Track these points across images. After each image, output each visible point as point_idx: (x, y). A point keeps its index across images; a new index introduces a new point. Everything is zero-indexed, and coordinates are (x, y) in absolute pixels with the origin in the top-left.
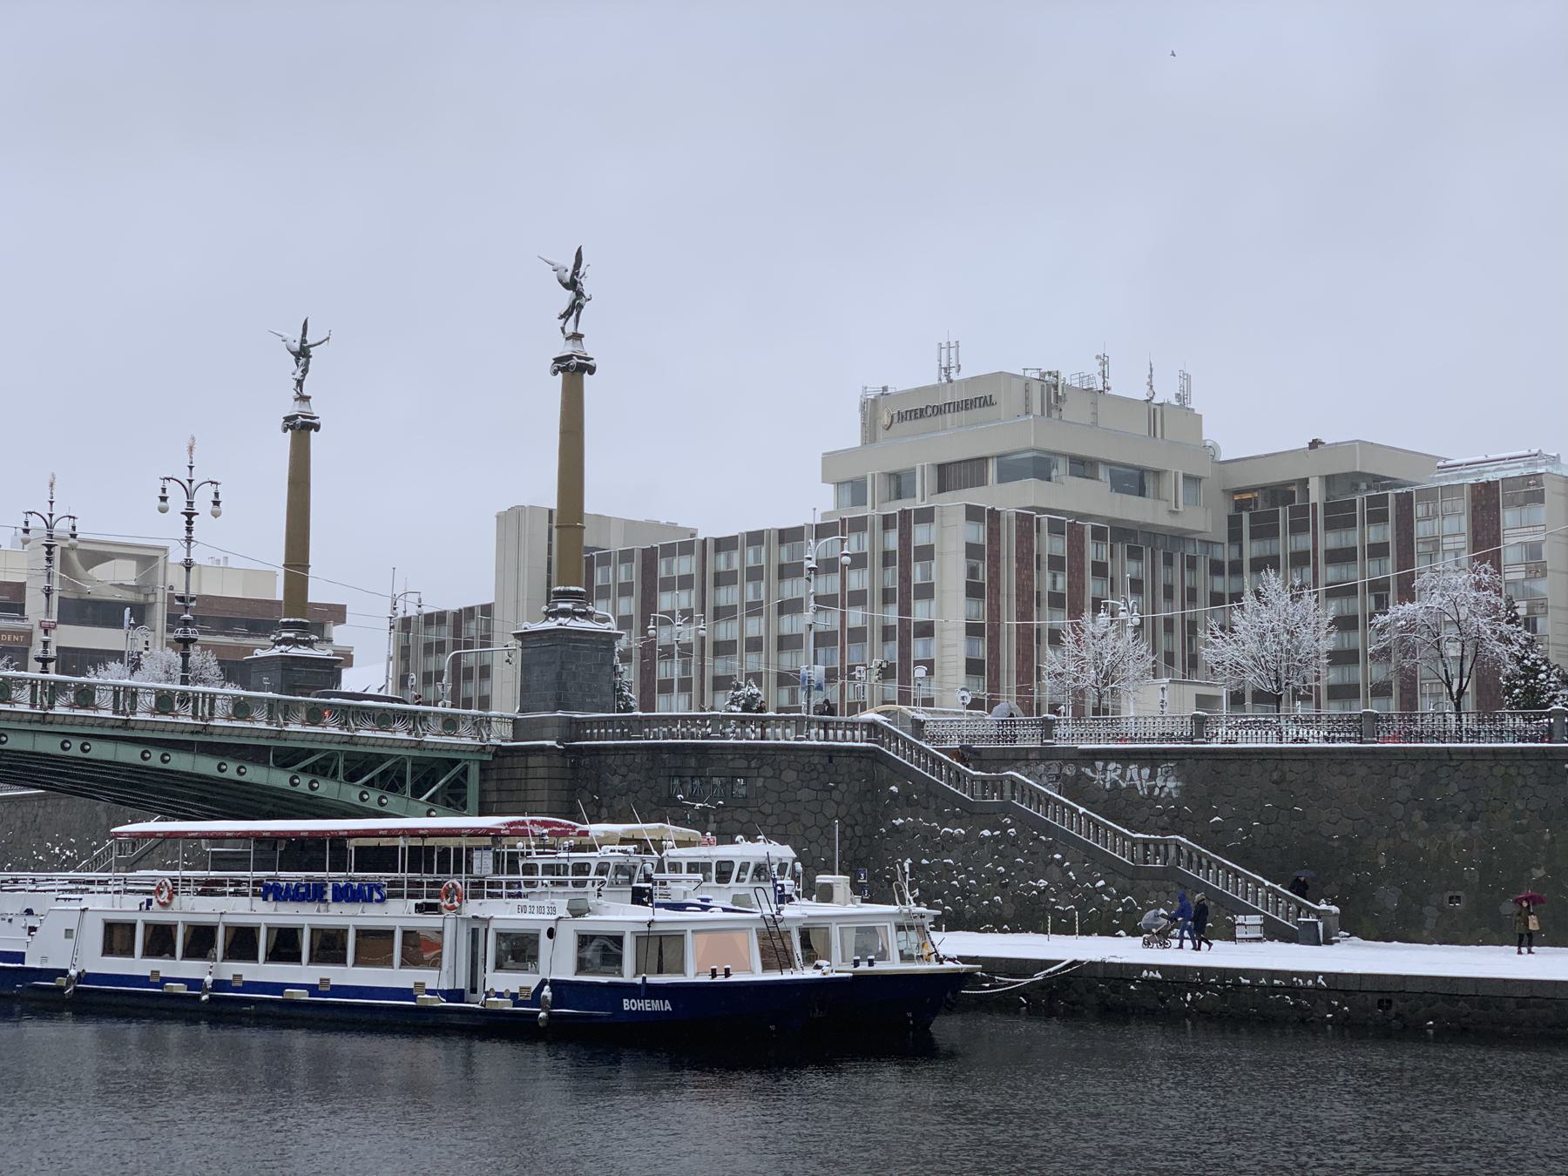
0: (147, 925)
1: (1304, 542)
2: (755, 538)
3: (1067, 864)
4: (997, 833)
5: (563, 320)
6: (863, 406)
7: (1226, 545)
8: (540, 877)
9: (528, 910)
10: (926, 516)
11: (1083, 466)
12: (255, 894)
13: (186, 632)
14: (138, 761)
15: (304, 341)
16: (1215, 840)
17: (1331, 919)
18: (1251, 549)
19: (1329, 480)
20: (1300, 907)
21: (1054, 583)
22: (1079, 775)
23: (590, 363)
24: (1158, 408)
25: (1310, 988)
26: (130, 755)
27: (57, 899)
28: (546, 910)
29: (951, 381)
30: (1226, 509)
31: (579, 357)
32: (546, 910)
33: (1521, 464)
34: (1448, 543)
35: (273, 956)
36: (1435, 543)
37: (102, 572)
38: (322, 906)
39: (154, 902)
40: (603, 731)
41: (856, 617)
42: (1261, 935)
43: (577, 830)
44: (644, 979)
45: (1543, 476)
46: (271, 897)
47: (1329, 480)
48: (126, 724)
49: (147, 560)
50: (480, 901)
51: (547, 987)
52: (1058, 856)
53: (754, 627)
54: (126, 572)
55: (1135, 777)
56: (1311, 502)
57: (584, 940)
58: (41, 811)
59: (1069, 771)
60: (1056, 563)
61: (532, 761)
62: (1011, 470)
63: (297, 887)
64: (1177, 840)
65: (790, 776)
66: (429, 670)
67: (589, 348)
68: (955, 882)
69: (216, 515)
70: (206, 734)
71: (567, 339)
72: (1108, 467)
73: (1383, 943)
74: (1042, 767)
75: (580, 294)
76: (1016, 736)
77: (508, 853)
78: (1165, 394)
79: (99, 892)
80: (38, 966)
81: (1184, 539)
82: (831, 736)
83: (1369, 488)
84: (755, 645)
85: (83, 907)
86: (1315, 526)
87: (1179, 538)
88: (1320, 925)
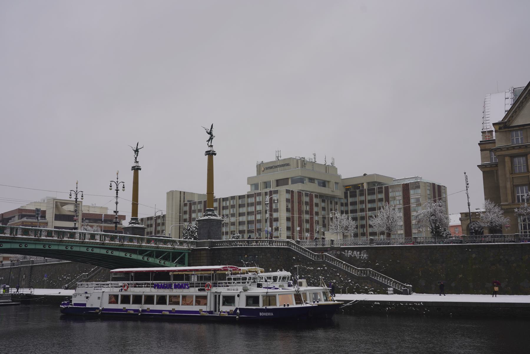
0: (122, 296)
1: (363, 198)
2: (233, 198)
3: (341, 276)
4: (322, 268)
5: (208, 142)
6: (257, 166)
7: (344, 199)
8: (232, 281)
9: (230, 290)
10: (276, 192)
11: (311, 180)
12: (152, 287)
13: (116, 220)
14: (106, 253)
15: (137, 148)
16: (377, 269)
17: (410, 288)
18: (350, 200)
19: (368, 183)
20: (402, 285)
21: (306, 208)
22: (341, 254)
23: (215, 152)
24: (327, 166)
25: (419, 305)
26: (104, 252)
27: (94, 289)
28: (235, 290)
29: (279, 160)
30: (344, 190)
31: (212, 151)
32: (235, 290)
33: (414, 179)
34: (397, 198)
35: (158, 303)
36: (394, 198)
38: (171, 290)
39: (123, 289)
40: (221, 244)
41: (258, 217)
42: (393, 293)
43: (238, 269)
44: (266, 307)
45: (420, 182)
46: (156, 288)
47: (368, 183)
48: (103, 244)
50: (216, 288)
51: (238, 310)
52: (338, 274)
53: (233, 219)
54: (71, 208)
55: (356, 254)
56: (364, 188)
57: (248, 298)
58: (60, 267)
59: (338, 253)
60: (307, 203)
61: (202, 252)
62: (295, 181)
63: (164, 285)
64: (369, 269)
65: (269, 255)
66: (148, 231)
67: (214, 149)
68: (311, 281)
69: (123, 190)
70: (122, 246)
71: (209, 147)
72: (317, 180)
73: (421, 294)
74: (331, 252)
75: (212, 135)
76: (317, 244)
78: (329, 163)
79: (106, 287)
80: (90, 307)
81: (334, 197)
82: (280, 245)
83: (378, 185)
84: (233, 224)
85: (103, 291)
87: (333, 197)
88: (408, 290)
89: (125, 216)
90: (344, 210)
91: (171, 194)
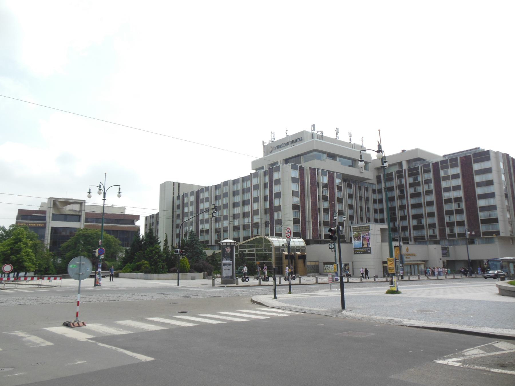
2: (225, 183)
7: (376, 185)
19: (409, 162)
37: (69, 207)
49: (81, 203)
54: (76, 207)
77: (255, 257)
86: (405, 176)
89: (139, 216)
90: (378, 209)
91: (163, 187)
